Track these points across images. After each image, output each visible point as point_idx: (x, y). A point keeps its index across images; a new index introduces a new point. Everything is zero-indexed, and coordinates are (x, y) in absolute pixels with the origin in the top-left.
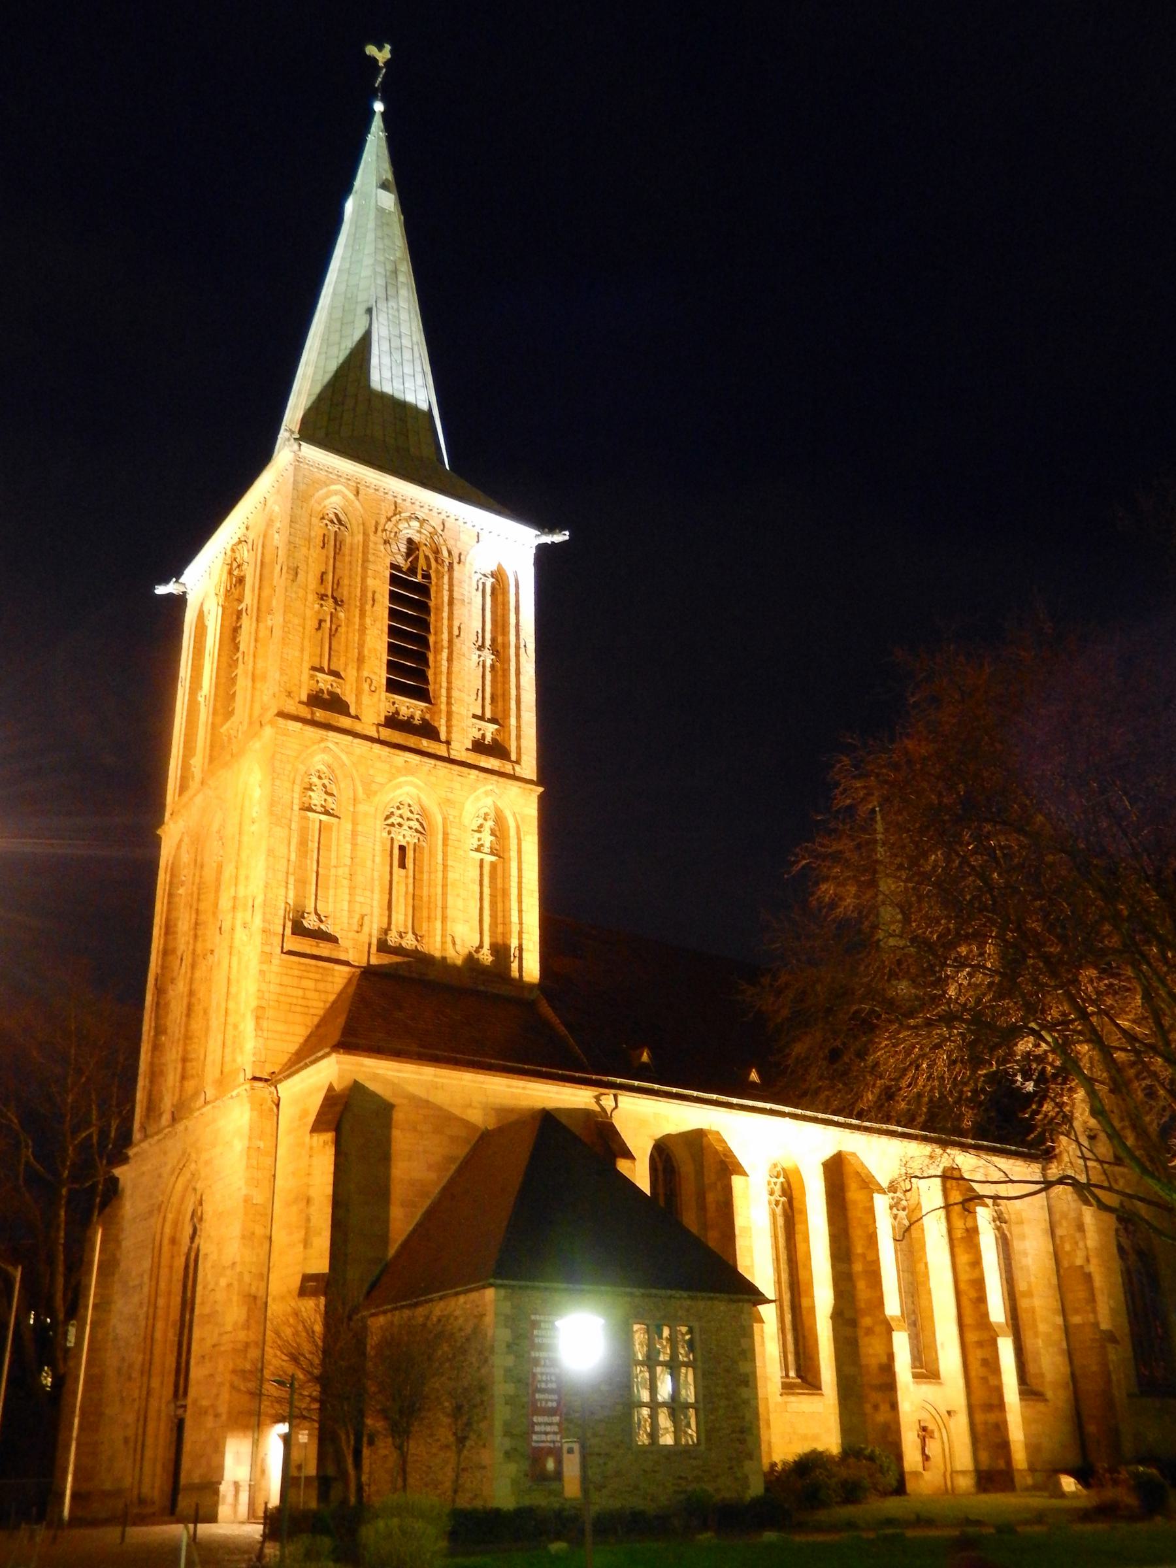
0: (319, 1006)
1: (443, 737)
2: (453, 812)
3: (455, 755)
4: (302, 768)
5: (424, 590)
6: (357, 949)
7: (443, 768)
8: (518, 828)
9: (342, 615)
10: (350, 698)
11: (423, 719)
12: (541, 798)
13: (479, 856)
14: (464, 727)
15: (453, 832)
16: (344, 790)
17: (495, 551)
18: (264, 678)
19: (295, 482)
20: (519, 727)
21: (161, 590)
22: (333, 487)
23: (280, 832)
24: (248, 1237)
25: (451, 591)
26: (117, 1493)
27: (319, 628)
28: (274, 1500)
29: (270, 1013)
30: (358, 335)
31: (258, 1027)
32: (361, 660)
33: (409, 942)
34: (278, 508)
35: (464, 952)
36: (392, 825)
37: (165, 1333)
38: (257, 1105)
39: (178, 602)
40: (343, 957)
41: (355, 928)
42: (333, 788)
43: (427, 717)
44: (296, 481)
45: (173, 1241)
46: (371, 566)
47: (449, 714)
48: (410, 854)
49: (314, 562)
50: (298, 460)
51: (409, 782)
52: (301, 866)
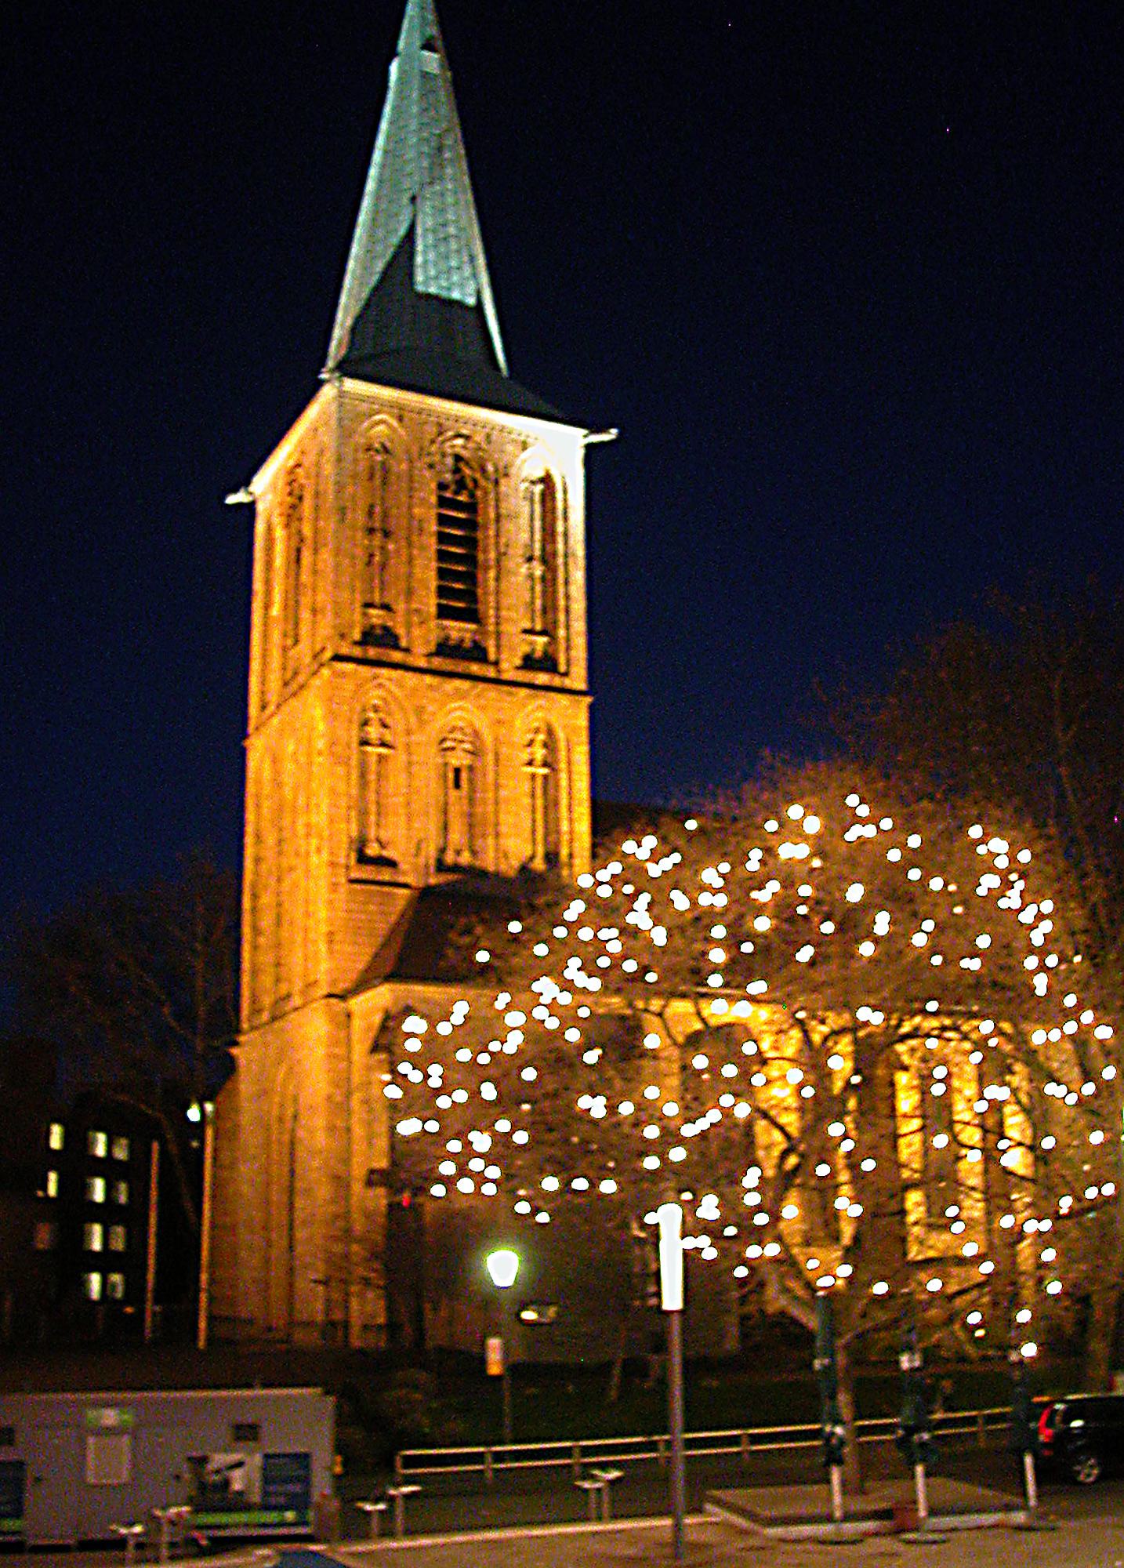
0: (383, 927)
1: (492, 656)
2: (503, 731)
3: (506, 676)
4: (358, 707)
5: (471, 507)
6: (414, 871)
7: (492, 693)
8: (568, 741)
9: (391, 547)
10: (401, 631)
11: (475, 642)
12: (592, 708)
13: (530, 770)
14: (513, 646)
15: (504, 750)
16: (397, 720)
17: (549, 453)
18: (323, 610)
19: (340, 420)
20: (568, 639)
21: (232, 499)
22: (377, 417)
23: (340, 770)
24: (331, 1129)
25: (497, 507)
26: (250, 1321)
27: (369, 563)
28: (319, 1390)
29: (337, 937)
30: (403, 231)
31: (331, 951)
32: (410, 593)
33: (465, 858)
34: (328, 439)
35: (515, 863)
36: (445, 750)
37: (277, 1195)
38: (333, 1019)
39: (250, 509)
40: (402, 879)
41: (413, 851)
42: (388, 721)
43: (478, 637)
44: (339, 416)
45: (281, 1119)
46: (417, 494)
47: (498, 635)
48: (464, 775)
49: (359, 495)
50: (342, 394)
51: (461, 708)
52: (363, 797)
